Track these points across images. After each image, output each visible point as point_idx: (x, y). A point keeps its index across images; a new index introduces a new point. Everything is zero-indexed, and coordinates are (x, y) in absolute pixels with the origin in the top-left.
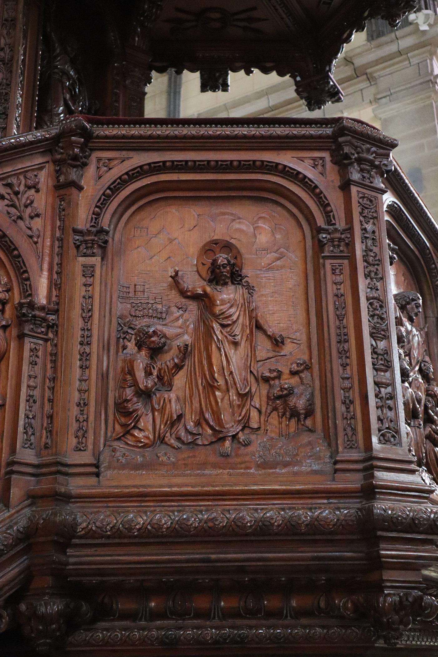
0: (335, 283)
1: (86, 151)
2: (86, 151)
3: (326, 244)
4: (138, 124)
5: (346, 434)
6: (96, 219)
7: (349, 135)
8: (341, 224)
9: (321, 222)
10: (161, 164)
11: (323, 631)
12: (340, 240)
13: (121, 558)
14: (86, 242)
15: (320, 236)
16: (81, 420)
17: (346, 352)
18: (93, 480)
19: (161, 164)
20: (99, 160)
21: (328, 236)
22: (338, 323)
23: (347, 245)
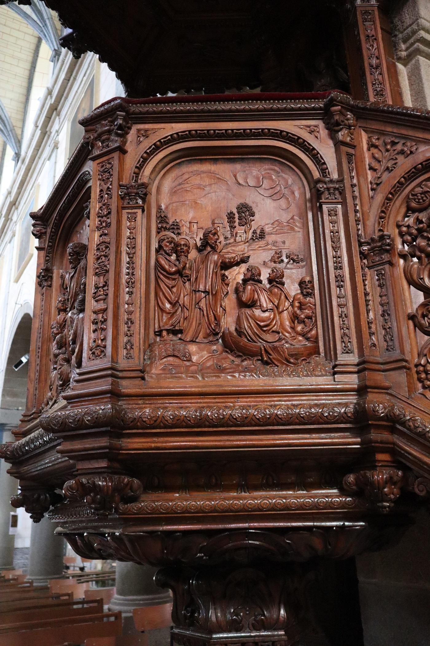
0: (331, 222)
1: (348, 115)
2: (348, 115)
3: (323, 192)
4: (175, 102)
5: (343, 341)
6: (136, 177)
7: (339, 105)
8: (335, 176)
9: (316, 175)
10: (187, 132)
11: (90, 496)
12: (335, 189)
13: (334, 440)
14: (328, 189)
15: (318, 186)
16: (129, 335)
17: (133, 283)
18: (138, 382)
19: (187, 132)
20: (139, 131)
21: (325, 186)
22: (128, 260)
23: (340, 193)
